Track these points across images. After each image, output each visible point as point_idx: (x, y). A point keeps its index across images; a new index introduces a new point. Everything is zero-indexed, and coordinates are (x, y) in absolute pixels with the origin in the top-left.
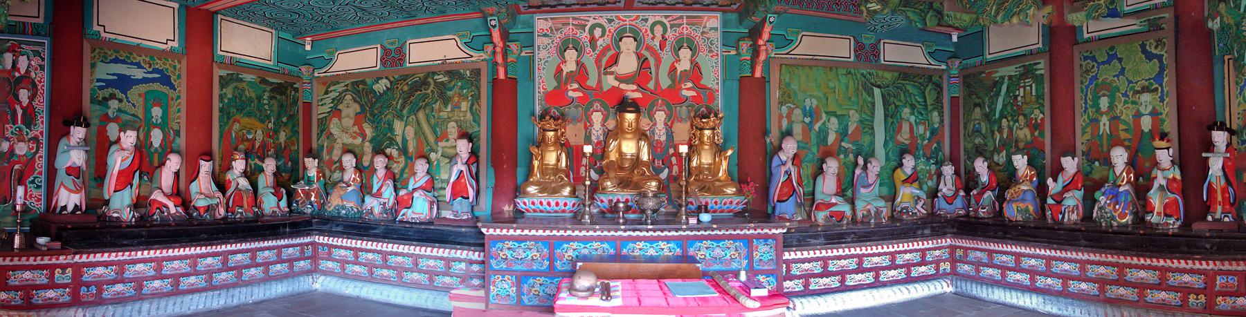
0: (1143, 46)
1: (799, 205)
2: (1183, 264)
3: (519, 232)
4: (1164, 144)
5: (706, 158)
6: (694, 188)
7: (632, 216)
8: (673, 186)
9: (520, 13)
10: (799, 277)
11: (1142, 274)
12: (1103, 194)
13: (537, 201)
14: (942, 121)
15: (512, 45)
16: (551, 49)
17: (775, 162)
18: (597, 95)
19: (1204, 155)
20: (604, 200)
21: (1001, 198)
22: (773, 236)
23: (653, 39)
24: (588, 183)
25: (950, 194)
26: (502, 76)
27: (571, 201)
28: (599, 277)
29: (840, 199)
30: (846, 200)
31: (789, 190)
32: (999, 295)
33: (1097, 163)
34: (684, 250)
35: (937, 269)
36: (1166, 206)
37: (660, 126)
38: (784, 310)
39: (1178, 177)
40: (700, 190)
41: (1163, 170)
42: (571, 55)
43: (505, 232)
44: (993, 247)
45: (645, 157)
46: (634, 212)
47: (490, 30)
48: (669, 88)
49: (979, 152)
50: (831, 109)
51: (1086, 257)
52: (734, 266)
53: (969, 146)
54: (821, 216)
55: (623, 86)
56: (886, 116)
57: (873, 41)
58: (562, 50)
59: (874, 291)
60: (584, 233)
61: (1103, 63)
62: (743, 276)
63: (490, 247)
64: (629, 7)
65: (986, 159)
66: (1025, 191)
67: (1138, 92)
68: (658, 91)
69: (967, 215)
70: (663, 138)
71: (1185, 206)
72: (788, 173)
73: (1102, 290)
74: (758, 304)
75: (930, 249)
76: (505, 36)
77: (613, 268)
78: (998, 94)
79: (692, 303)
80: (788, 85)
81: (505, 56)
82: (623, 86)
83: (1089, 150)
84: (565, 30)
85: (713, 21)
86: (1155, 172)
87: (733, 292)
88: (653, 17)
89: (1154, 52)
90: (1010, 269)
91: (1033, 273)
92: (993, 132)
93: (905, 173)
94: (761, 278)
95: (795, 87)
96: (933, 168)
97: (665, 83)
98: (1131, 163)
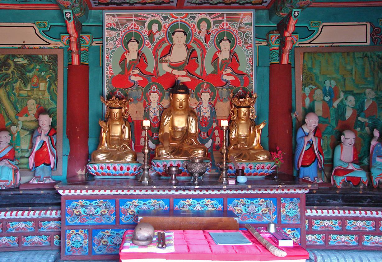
1: (320, 170)
3: (90, 192)
5: (243, 131)
6: (232, 155)
7: (182, 178)
8: (216, 154)
9: (91, 8)
10: (320, 233)
13: (105, 166)
15: (85, 36)
16: (118, 41)
17: (300, 134)
18: (154, 79)
20: (159, 165)
22: (297, 196)
23: (199, 33)
24: (146, 151)
26: (76, 62)
27: (133, 166)
28: (156, 228)
31: (310, 157)
34: (225, 206)
37: (205, 105)
40: (238, 157)
42: (133, 46)
43: (73, 192)
45: (193, 130)
46: (184, 175)
47: (65, 22)
48: (213, 74)
50: (348, 89)
52: (265, 220)
54: (339, 180)
55: (175, 72)
58: (126, 42)
60: (143, 192)
62: (272, 229)
63: (66, 206)
64: (180, 6)
68: (203, 76)
70: (208, 115)
72: (310, 143)
74: (284, 254)
76: (79, 28)
77: (167, 221)
79: (232, 251)
80: (310, 69)
81: (78, 45)
82: (175, 72)
84: (129, 25)
85: (248, 17)
87: (264, 242)
88: (200, 14)
94: (287, 231)
95: (316, 71)
97: (209, 69)
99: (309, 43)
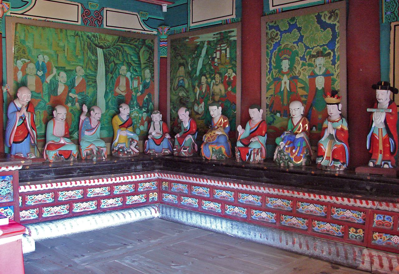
0: (319, 17)
1: (33, 146)
2: (346, 202)
4: (334, 100)
11: (312, 207)
12: (283, 140)
14: (152, 77)
17: (11, 108)
19: (369, 110)
21: (199, 141)
22: (10, 173)
25: (158, 137)
29: (68, 140)
30: (73, 141)
32: (196, 220)
33: (278, 115)
35: (147, 198)
36: (334, 152)
38: (20, 236)
39: (346, 128)
41: (333, 122)
44: (192, 180)
49: (183, 103)
50: (61, 65)
51: (266, 191)
53: (175, 98)
54: (52, 155)
56: (107, 72)
57: (97, 8)
59: (97, 217)
61: (285, 32)
65: (188, 109)
66: (219, 136)
67: (314, 56)
69: (172, 154)
71: (351, 152)
72: (23, 118)
73: (278, 219)
75: (141, 182)
78: (199, 56)
80: (23, 42)
83: (272, 103)
86: (327, 124)
89: (328, 22)
90: (206, 199)
91: (223, 202)
92: (194, 87)
93: (121, 119)
95: (29, 44)
96: (145, 115)
98: (306, 115)
99: (22, 14)
